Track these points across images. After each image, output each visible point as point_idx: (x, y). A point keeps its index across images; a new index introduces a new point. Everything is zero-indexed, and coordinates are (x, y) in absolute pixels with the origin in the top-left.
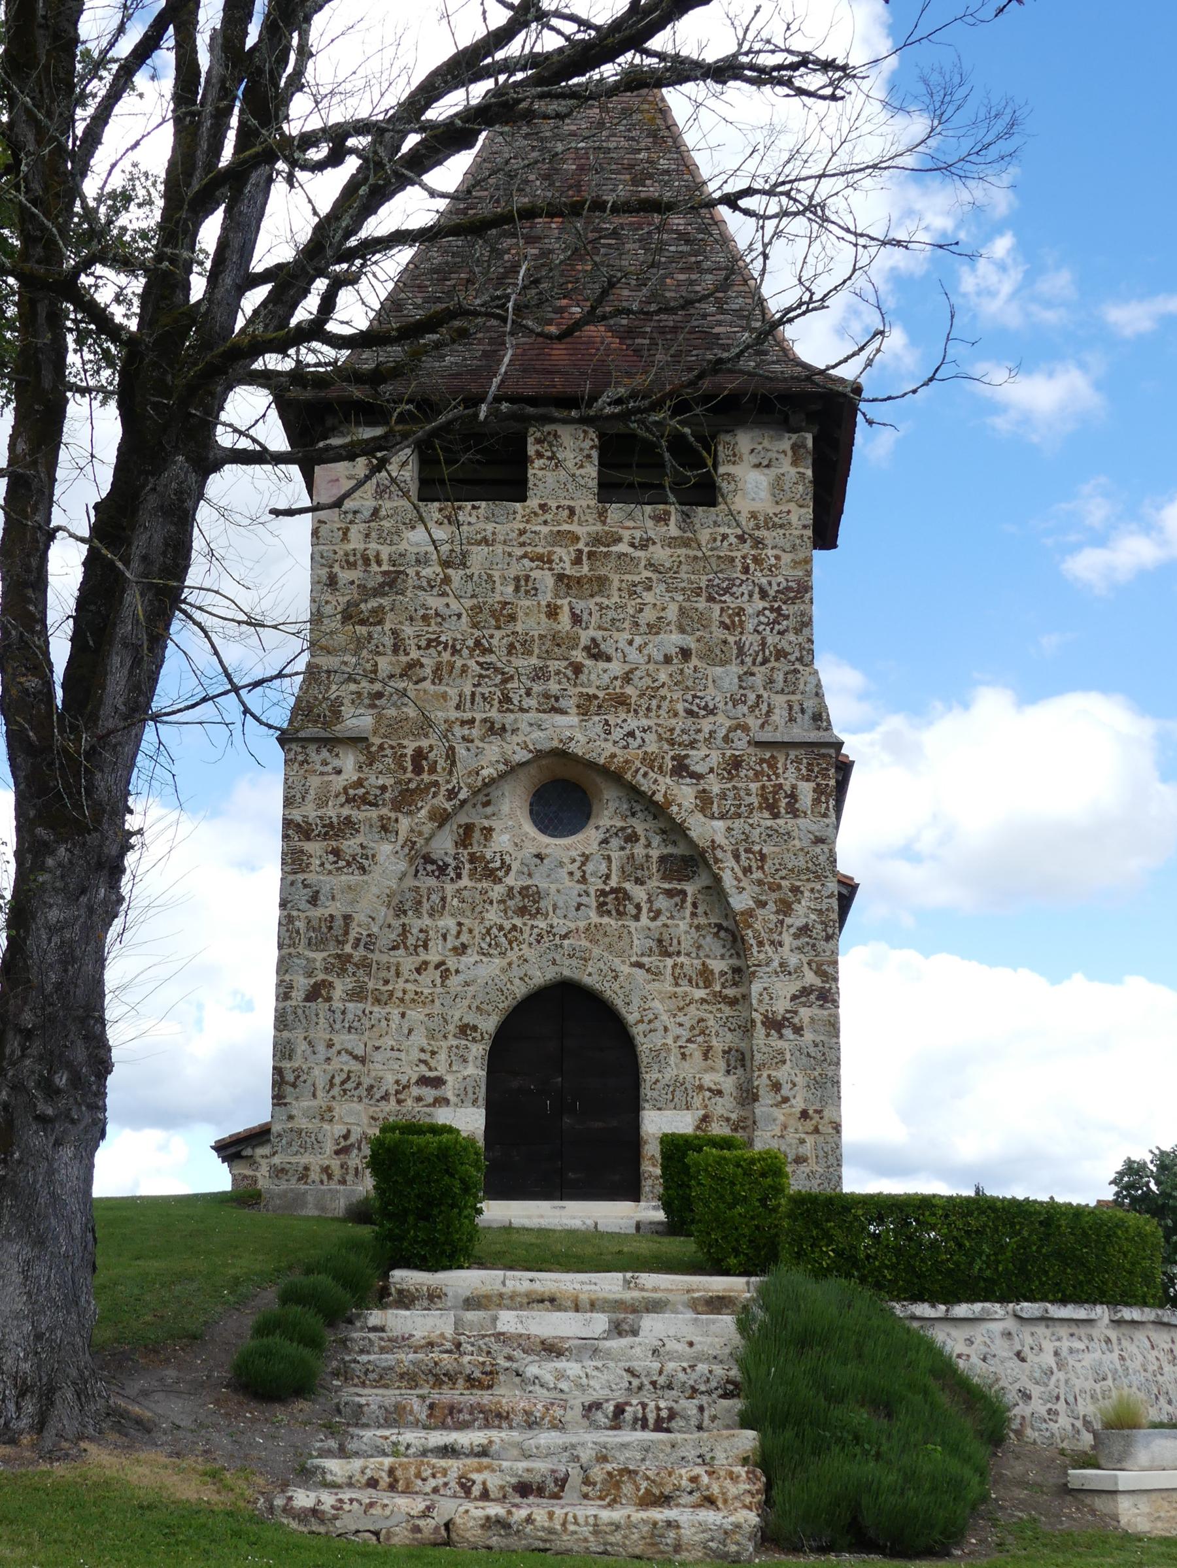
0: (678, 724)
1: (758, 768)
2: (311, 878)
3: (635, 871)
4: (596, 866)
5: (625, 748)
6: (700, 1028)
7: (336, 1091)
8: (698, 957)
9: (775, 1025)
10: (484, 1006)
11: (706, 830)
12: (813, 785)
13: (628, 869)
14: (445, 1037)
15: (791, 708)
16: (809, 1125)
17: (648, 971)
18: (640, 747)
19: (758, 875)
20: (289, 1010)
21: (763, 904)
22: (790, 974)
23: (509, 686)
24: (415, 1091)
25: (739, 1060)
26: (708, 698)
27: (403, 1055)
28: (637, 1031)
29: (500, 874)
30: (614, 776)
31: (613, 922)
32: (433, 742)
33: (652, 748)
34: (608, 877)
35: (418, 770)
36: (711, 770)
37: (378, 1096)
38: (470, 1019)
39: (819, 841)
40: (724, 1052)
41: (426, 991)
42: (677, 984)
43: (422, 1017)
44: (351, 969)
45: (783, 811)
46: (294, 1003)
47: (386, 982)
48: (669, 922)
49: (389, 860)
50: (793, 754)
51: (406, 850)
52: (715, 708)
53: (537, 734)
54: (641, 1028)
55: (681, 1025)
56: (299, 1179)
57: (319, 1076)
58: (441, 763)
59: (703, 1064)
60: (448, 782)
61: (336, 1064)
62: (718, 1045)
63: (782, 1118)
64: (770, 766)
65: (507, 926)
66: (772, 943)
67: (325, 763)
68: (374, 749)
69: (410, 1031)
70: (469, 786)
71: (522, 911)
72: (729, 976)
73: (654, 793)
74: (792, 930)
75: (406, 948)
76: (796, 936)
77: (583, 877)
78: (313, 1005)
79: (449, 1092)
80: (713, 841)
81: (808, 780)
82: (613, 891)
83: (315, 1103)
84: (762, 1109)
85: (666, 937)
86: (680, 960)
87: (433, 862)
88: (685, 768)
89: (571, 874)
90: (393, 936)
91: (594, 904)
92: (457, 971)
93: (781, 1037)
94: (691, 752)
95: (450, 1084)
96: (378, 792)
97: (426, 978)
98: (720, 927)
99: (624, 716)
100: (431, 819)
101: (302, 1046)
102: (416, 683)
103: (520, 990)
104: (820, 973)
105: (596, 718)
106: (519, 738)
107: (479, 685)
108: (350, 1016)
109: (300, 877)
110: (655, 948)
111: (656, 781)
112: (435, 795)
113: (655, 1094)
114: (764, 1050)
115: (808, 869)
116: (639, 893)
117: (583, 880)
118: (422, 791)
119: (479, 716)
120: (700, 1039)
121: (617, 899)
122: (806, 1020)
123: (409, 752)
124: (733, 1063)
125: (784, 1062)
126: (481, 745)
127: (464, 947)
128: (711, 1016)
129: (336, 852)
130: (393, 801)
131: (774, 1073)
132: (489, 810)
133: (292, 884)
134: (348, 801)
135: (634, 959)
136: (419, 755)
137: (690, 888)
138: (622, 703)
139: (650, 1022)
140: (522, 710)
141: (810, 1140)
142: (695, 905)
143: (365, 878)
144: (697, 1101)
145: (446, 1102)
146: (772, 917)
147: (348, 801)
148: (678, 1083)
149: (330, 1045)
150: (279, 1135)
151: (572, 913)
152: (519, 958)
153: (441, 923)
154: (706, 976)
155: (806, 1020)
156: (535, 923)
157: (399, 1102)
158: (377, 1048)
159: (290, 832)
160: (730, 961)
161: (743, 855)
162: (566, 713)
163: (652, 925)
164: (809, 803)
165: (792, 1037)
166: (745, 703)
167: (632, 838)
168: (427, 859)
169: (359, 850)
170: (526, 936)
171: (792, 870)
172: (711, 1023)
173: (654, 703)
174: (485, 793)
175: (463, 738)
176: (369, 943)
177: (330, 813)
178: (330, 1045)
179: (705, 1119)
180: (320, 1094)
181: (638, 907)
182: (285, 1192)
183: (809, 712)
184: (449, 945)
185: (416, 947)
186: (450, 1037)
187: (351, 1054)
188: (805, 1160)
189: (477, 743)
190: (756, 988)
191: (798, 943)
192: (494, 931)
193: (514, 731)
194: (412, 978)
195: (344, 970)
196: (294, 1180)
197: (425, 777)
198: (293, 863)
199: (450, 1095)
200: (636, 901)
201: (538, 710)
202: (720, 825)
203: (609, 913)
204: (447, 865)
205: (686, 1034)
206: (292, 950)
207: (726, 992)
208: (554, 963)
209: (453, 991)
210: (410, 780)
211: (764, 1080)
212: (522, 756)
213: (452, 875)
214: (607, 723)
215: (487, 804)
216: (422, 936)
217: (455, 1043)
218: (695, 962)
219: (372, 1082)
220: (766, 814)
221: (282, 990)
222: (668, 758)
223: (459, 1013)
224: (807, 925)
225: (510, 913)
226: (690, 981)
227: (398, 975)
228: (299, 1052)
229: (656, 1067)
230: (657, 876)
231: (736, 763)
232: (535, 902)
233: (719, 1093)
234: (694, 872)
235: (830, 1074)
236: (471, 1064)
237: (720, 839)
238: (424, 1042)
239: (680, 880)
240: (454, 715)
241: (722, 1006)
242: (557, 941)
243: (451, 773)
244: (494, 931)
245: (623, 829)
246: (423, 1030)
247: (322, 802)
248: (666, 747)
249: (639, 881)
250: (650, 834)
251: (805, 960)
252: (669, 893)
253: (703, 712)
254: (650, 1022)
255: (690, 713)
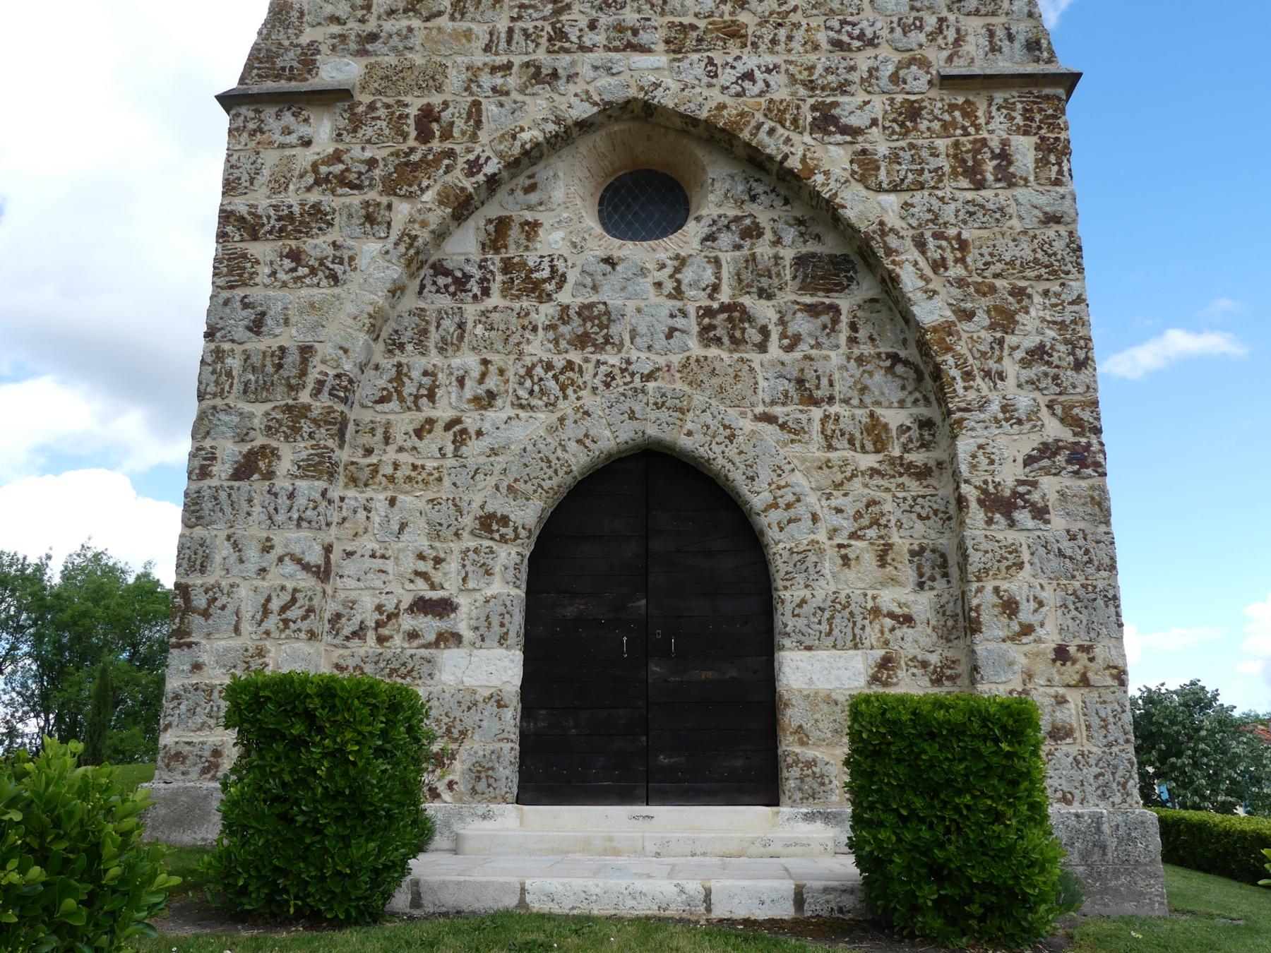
0: (821, 60)
1: (947, 117)
2: (255, 294)
3: (759, 280)
4: (698, 273)
5: (738, 95)
6: (871, 517)
7: (272, 622)
8: (862, 404)
9: (1001, 504)
10: (520, 486)
11: (864, 207)
12: (1035, 139)
13: (747, 276)
14: (457, 534)
15: (991, 34)
16: (1071, 672)
17: (783, 427)
18: (761, 94)
19: (956, 271)
20: (207, 493)
21: (969, 315)
22: (1020, 422)
23: (564, 18)
24: (408, 622)
25: (943, 565)
26: (865, 24)
27: (389, 565)
28: (769, 522)
29: (549, 287)
30: (720, 138)
31: (725, 355)
32: (449, 97)
33: (781, 92)
34: (716, 288)
35: (424, 135)
36: (874, 122)
37: (347, 631)
38: (498, 505)
39: (1052, 219)
40: (913, 553)
41: (430, 464)
42: (830, 447)
43: (421, 504)
44: (306, 427)
45: (990, 177)
46: (214, 482)
47: (369, 452)
48: (814, 352)
49: (376, 266)
50: (999, 97)
51: (402, 248)
52: (875, 36)
53: (605, 81)
54: (775, 516)
55: (839, 511)
56: (205, 771)
57: (247, 598)
58: (460, 124)
59: (879, 573)
60: (469, 151)
61: (275, 578)
62: (901, 542)
63: (1024, 660)
64: (965, 115)
65: (559, 362)
66: (987, 374)
67: (287, 131)
68: (360, 109)
69: (403, 526)
70: (500, 155)
71: (582, 341)
72: (915, 433)
73: (786, 157)
74: (1019, 355)
75: (402, 399)
76: (1025, 363)
77: (678, 289)
78: (244, 485)
79: (461, 622)
80: (882, 223)
81: (1026, 133)
82: (724, 308)
83: (236, 643)
84: (989, 643)
85: (809, 374)
86: (835, 409)
87: (447, 273)
88: (835, 120)
89: (659, 285)
90: (382, 383)
91: (695, 329)
92: (479, 433)
93: (1012, 524)
94: (841, 99)
95: (464, 610)
96: (363, 168)
97: (429, 445)
98: (895, 358)
99: (737, 52)
100: (441, 203)
101: (223, 551)
102: (427, 19)
103: (578, 459)
104: (1068, 419)
105: (695, 56)
106: (579, 87)
107: (520, 18)
108: (301, 501)
109: (239, 292)
110: (792, 392)
111: (788, 140)
112: (448, 169)
113: (801, 623)
114: (985, 545)
115: (1036, 261)
116: (765, 311)
117: (678, 293)
118: (426, 165)
119: (517, 60)
120: (872, 533)
121: (730, 319)
122: (1053, 497)
123: (413, 111)
124: (927, 571)
125: (1020, 566)
126: (520, 98)
127: (491, 395)
128: (888, 496)
129: (295, 256)
130: (386, 179)
131: (1004, 585)
132: (533, 198)
133: (226, 303)
134: (317, 182)
135: (759, 409)
136: (427, 116)
137: (845, 303)
138: (733, 35)
139: (789, 506)
140: (583, 48)
141: (1074, 697)
142: (853, 327)
143: (336, 290)
144: (872, 634)
145: (457, 639)
146: (983, 334)
147: (317, 182)
148: (838, 605)
149: (267, 548)
150: (177, 697)
151: (660, 342)
152: (577, 410)
153: (456, 362)
154: (876, 434)
155: (1053, 497)
156: (602, 358)
157: (381, 640)
158: (350, 554)
159: (229, 229)
160: (916, 411)
161: (931, 243)
162: (649, 51)
163: (787, 358)
164: (1031, 166)
165: (1031, 524)
166: (921, 28)
167: (753, 232)
168: (439, 269)
169: (330, 251)
170: (587, 377)
171: (1011, 263)
172: (888, 506)
173: (782, 33)
174: (526, 162)
175: (494, 89)
176: (344, 388)
177: (291, 201)
178: (267, 548)
179: (886, 663)
180: (246, 627)
181: (764, 331)
182: (176, 794)
183: (1021, 38)
184: (468, 394)
185: (417, 397)
186: (465, 535)
187: (299, 561)
188: (1069, 733)
189: (515, 95)
190: (965, 446)
191: (1031, 373)
192: (539, 371)
193: (570, 78)
194: (408, 444)
195: (296, 430)
196: (194, 775)
197: (436, 145)
198: (230, 273)
199: (463, 628)
200: (761, 322)
201: (608, 49)
202: (892, 200)
203: (718, 341)
204: (468, 277)
205: (847, 525)
206: (218, 402)
207: (909, 457)
208: (632, 416)
209: (472, 463)
210: (412, 150)
211: (988, 597)
212: (583, 111)
213: (476, 290)
214: (711, 61)
215: (531, 188)
216: (427, 381)
217: (472, 544)
218: (858, 412)
219: (340, 609)
220: (964, 183)
221: (197, 463)
222: (805, 108)
223: (482, 497)
224: (1041, 346)
225: (563, 344)
226: (851, 441)
227: (387, 440)
228: (218, 559)
229: (801, 579)
230: (792, 285)
231: (913, 112)
232: (602, 327)
233: (908, 620)
234: (851, 279)
235: (1100, 585)
236: (497, 578)
237: (892, 220)
238: (423, 544)
239: (829, 291)
240: (480, 59)
241: (905, 479)
242: (637, 382)
243: (474, 137)
244: (539, 371)
245: (737, 219)
246: (422, 523)
247: (280, 184)
248: (802, 92)
249: (765, 294)
250: (781, 225)
251: (1043, 401)
252: (813, 311)
253: (856, 44)
254: (789, 506)
255: (838, 45)
